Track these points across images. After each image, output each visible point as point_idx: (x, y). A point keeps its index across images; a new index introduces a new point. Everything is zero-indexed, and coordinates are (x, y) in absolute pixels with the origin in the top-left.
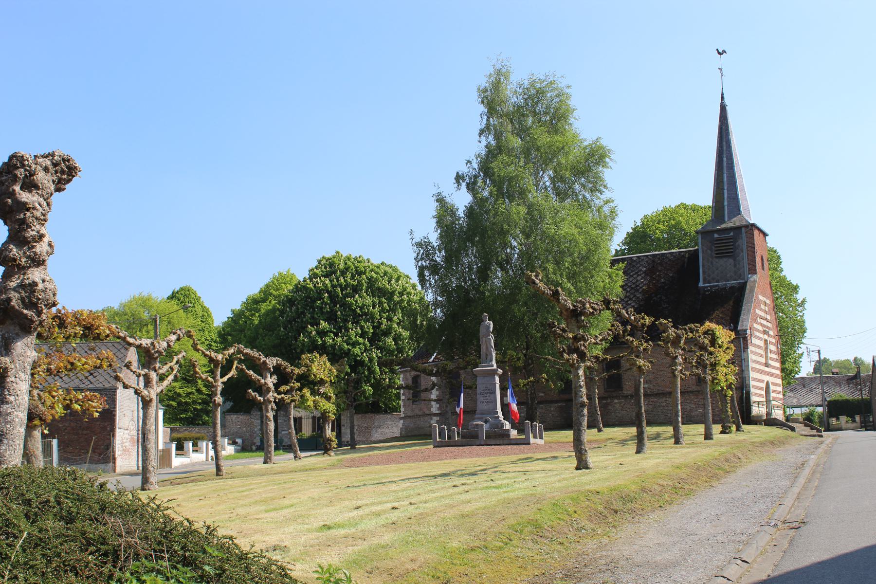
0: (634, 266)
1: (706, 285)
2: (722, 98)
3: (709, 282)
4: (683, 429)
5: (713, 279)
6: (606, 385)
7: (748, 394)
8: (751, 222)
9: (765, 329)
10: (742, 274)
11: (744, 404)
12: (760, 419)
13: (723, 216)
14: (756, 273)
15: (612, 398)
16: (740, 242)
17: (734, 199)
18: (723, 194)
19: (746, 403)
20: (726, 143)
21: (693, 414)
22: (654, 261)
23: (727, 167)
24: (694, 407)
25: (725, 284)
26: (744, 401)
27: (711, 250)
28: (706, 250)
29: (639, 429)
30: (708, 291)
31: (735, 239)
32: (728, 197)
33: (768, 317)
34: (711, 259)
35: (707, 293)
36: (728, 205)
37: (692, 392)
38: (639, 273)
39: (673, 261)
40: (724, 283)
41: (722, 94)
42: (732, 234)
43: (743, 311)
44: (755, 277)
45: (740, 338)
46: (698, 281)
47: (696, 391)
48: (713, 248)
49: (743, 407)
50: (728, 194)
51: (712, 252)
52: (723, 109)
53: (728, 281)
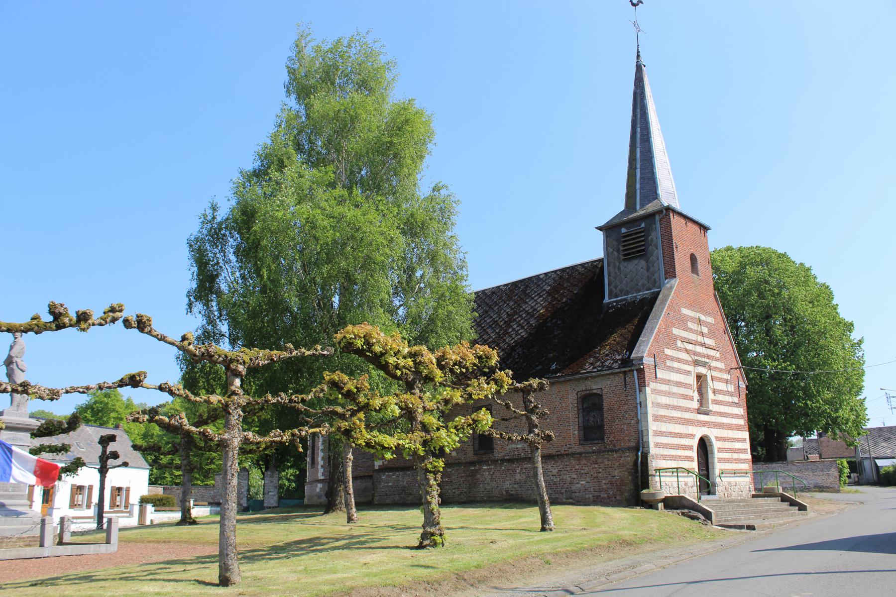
0: (539, 285)
1: (612, 300)
2: (638, 56)
3: (616, 297)
4: (449, 516)
5: (621, 291)
6: (477, 445)
7: (645, 456)
8: (666, 204)
9: (696, 358)
10: (657, 280)
11: (639, 474)
12: (652, 499)
13: (635, 204)
14: (675, 277)
15: (481, 462)
16: (653, 235)
17: (649, 179)
18: (635, 176)
19: (642, 472)
20: (641, 110)
21: (574, 488)
22: (561, 277)
23: (641, 139)
24: (575, 476)
25: (635, 296)
26: (639, 468)
27: (618, 251)
28: (612, 252)
29: (94, 531)
30: (613, 307)
31: (646, 232)
32: (641, 178)
33: (710, 342)
34: (617, 264)
35: (611, 311)
36: (641, 188)
37: (573, 454)
38: (541, 294)
39: (583, 274)
40: (635, 295)
41: (638, 52)
42: (643, 225)
43: (644, 331)
44: (673, 281)
45: (633, 371)
46: (604, 298)
47: (577, 454)
48: (620, 246)
49: (637, 477)
50: (641, 173)
51: (619, 253)
52: (639, 69)
53: (639, 291)
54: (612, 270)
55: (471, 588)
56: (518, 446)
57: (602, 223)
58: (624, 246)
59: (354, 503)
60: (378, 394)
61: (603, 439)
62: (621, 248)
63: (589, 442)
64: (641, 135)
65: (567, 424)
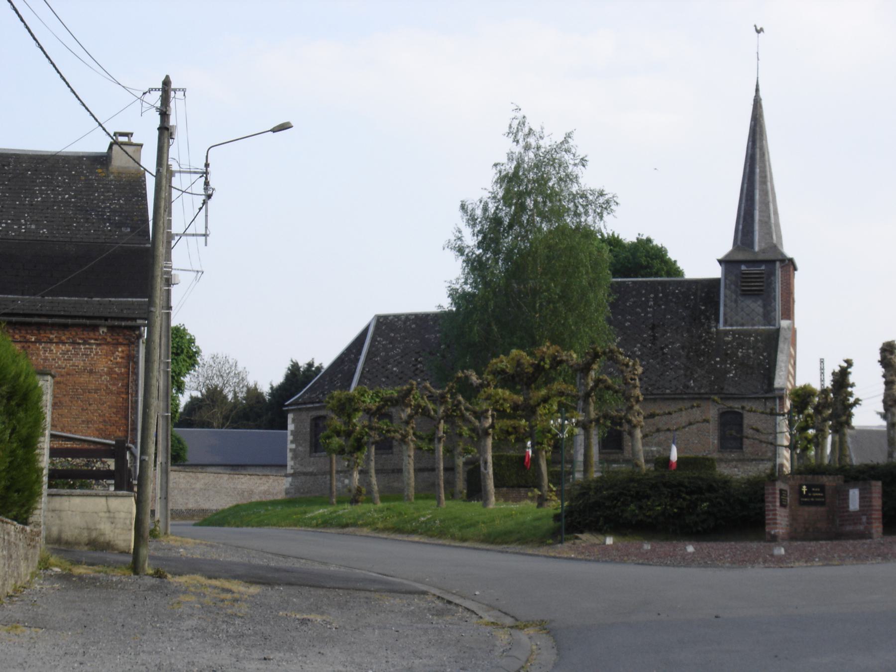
2: (757, 90)
54: (728, 302)
55: (527, 121)
56: (652, 449)
57: (721, 256)
58: (763, 278)
59: (442, 468)
60: (136, 489)
61: (741, 448)
62: (739, 283)
63: (728, 450)
64: (760, 177)
65: (707, 434)
